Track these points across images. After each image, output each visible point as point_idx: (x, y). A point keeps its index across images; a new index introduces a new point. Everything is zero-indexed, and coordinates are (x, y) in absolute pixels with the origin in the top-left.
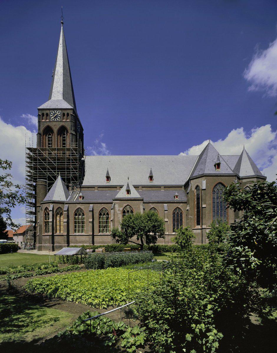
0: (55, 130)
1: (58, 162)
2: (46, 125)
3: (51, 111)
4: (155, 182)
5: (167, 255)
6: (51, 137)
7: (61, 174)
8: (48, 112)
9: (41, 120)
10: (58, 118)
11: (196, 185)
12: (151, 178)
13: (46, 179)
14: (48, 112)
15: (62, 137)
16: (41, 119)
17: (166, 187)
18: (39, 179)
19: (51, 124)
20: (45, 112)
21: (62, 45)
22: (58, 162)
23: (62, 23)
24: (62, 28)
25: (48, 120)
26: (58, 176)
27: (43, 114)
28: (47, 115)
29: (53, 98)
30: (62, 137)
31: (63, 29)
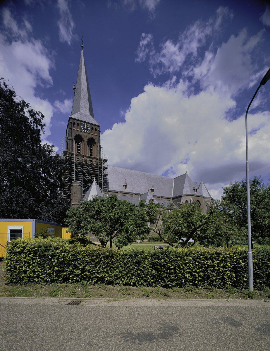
0: (86, 139)
1: (92, 169)
2: (77, 133)
3: (81, 122)
4: (128, 190)
5: (96, 244)
6: (92, 147)
7: (95, 179)
8: (79, 122)
9: (73, 128)
10: (88, 131)
11: (186, 200)
12: (125, 186)
13: (81, 181)
14: (79, 122)
15: (76, 144)
16: (73, 127)
17: (137, 194)
18: (76, 180)
19: (81, 134)
20: (76, 122)
21: (84, 66)
22: (92, 169)
23: (82, 47)
24: (82, 51)
25: (78, 130)
26: (93, 180)
27: (74, 123)
28: (78, 124)
29: (81, 111)
30: (89, 147)
31: (83, 52)
